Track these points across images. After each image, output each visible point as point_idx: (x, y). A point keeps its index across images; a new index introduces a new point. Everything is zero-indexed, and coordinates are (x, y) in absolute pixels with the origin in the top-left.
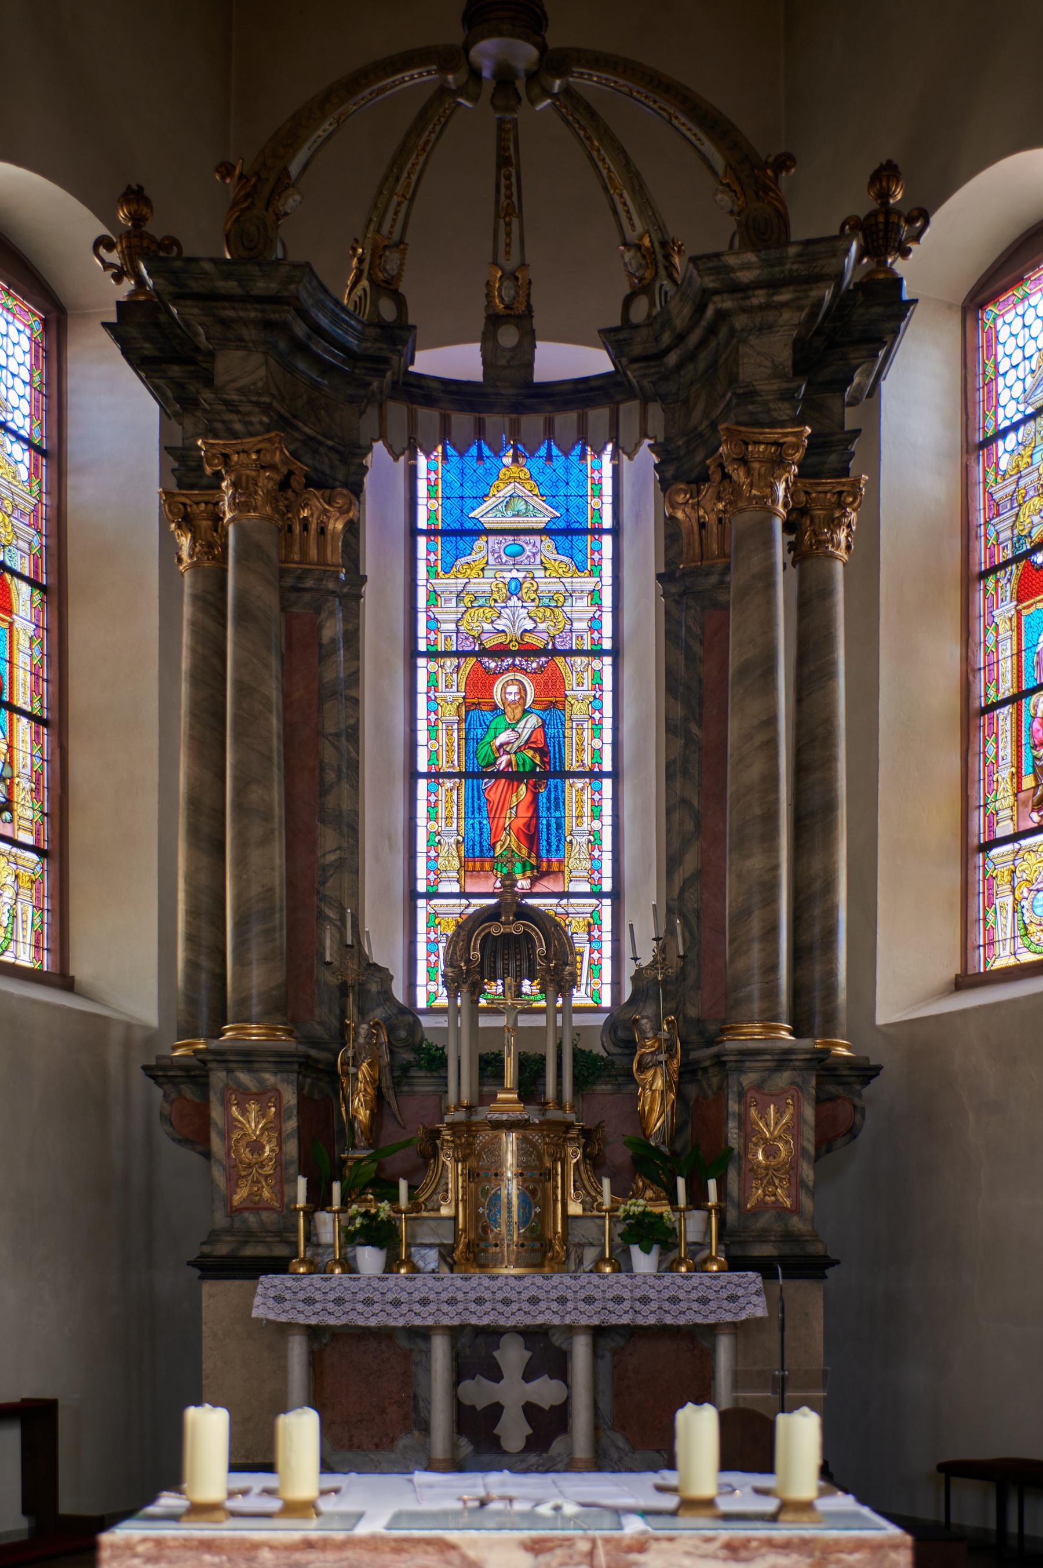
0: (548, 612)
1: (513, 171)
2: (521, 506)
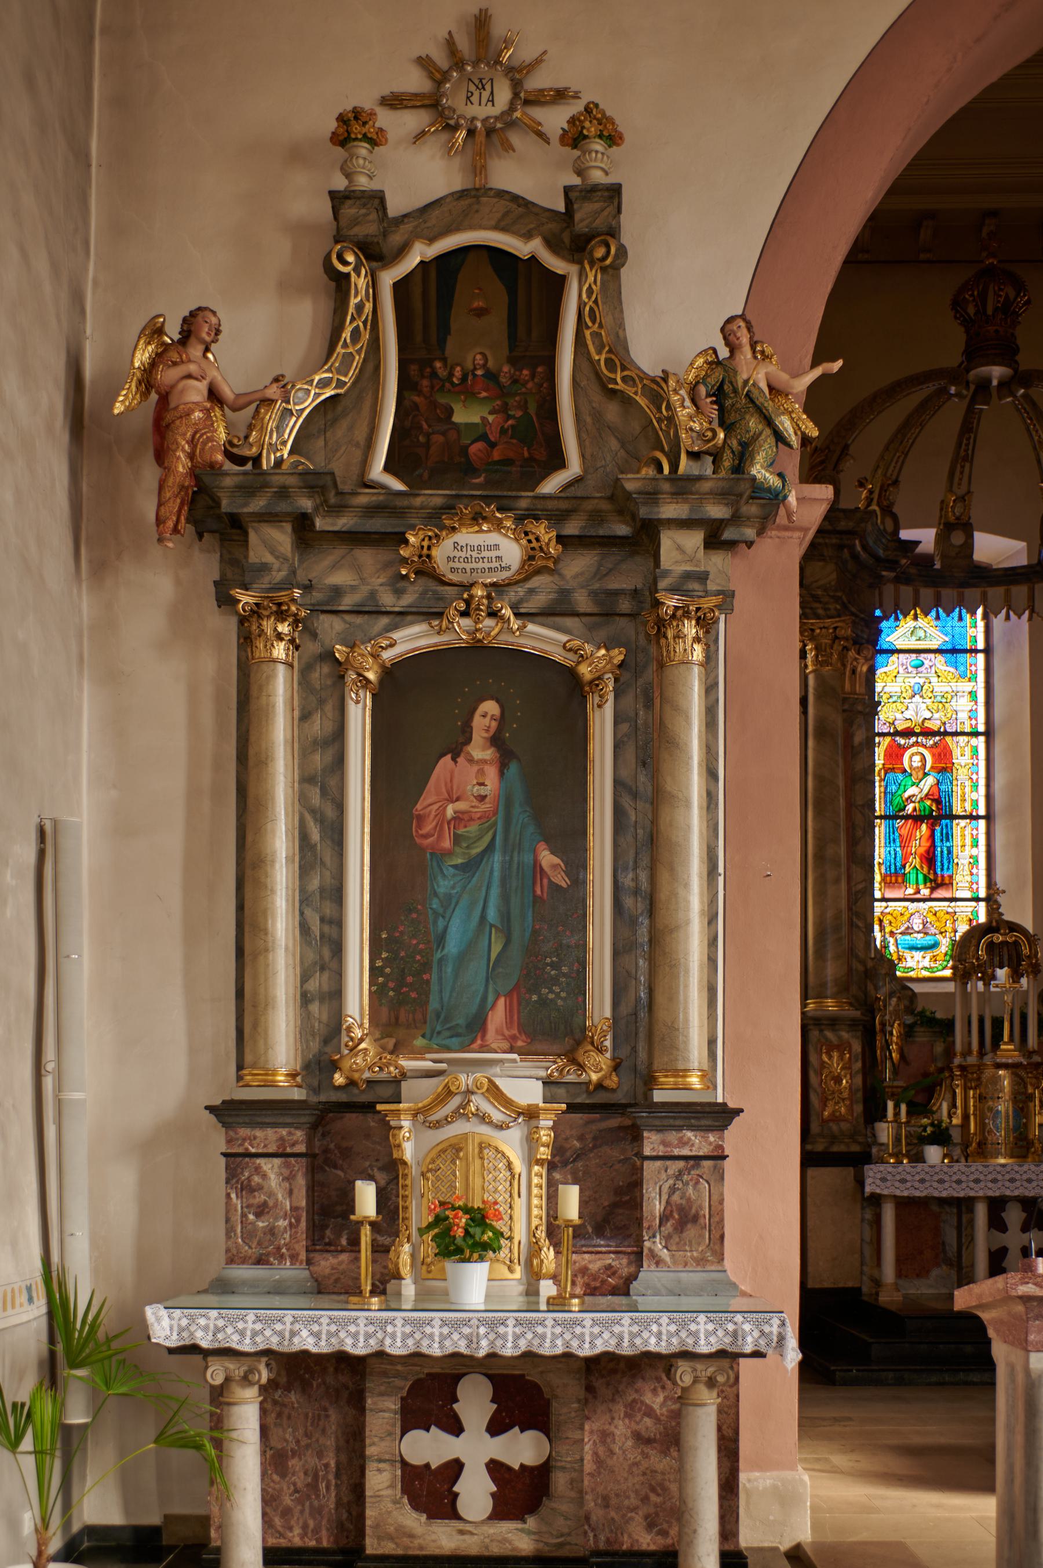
0: (941, 706)
1: (972, 436)
2: (921, 633)
